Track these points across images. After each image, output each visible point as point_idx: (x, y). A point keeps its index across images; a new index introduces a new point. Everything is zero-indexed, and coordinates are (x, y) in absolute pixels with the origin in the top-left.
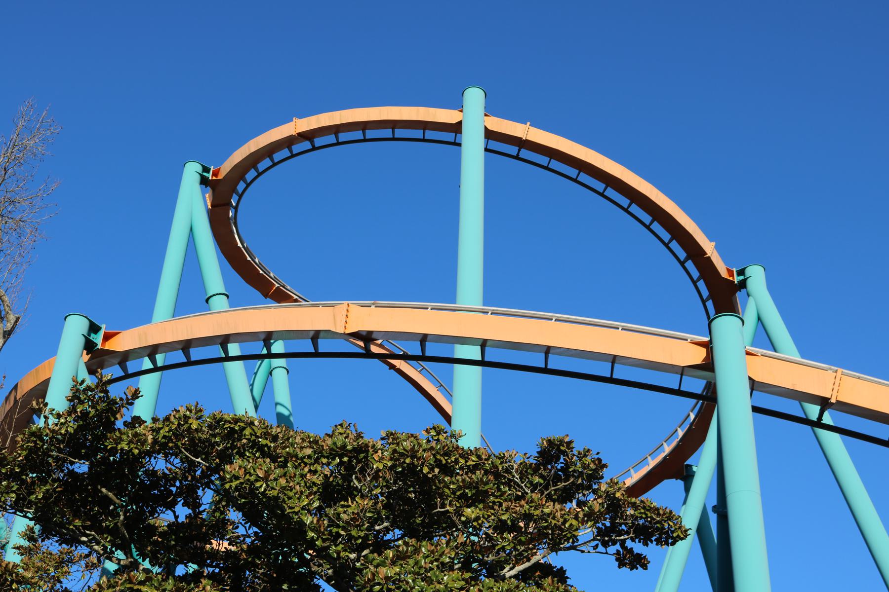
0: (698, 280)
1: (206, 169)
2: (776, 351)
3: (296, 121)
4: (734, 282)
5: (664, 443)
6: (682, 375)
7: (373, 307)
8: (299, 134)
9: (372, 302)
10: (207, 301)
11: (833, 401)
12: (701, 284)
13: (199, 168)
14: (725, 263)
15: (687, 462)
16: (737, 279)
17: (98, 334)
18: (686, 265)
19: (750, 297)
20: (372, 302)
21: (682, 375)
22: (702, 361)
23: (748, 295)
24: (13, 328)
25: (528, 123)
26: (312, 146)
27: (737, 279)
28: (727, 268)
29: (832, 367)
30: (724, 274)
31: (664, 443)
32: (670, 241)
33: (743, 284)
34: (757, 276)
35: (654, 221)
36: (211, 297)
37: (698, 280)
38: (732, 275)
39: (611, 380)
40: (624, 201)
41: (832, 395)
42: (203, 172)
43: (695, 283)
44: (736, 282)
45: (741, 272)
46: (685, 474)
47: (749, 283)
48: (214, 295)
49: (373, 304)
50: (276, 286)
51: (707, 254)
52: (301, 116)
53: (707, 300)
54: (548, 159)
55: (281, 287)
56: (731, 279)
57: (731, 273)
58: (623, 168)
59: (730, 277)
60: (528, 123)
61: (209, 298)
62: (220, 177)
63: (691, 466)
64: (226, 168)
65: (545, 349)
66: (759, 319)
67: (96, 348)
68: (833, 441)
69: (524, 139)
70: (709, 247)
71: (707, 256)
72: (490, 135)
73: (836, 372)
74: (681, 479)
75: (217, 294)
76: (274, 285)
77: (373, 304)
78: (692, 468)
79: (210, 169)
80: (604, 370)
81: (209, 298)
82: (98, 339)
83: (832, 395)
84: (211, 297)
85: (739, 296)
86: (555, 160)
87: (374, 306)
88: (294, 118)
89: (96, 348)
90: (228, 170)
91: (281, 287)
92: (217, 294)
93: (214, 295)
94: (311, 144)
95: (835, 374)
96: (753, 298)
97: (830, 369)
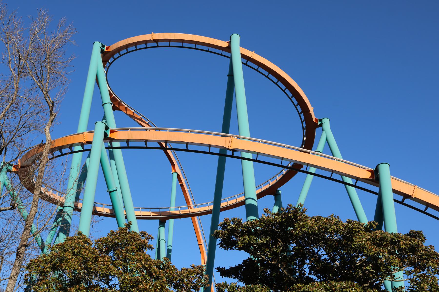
0: (297, 105)
1: (103, 46)
2: (333, 156)
3: (153, 34)
4: (318, 124)
5: (270, 180)
6: (282, 160)
7: (236, 138)
8: (154, 40)
9: (236, 135)
10: (103, 105)
11: (413, 197)
12: (298, 107)
13: (100, 45)
14: (315, 116)
15: (278, 189)
16: (319, 123)
17: (107, 130)
18: (301, 115)
19: (324, 131)
20: (236, 135)
21: (282, 160)
22: (370, 177)
23: (323, 130)
24: (54, 119)
25: (254, 52)
26: (157, 45)
27: (319, 123)
28: (315, 118)
29: (409, 183)
30: (314, 120)
31: (270, 180)
32: (285, 89)
33: (321, 125)
34: (327, 123)
35: (158, 43)
36: (105, 104)
37: (297, 105)
38: (317, 122)
39: (330, 179)
40: (266, 73)
41: (413, 195)
42: (102, 47)
43: (296, 106)
44: (318, 124)
45: (321, 120)
46: (276, 194)
47: (324, 125)
48: (107, 103)
49: (236, 136)
50: (113, 96)
51: (310, 112)
52: (155, 32)
53: (304, 121)
54: (222, 51)
55: (116, 97)
56: (316, 122)
57: (316, 120)
58: (287, 74)
59: (316, 121)
60: (254, 52)
61: (104, 104)
62: (108, 50)
63: (278, 190)
64: (113, 47)
65: (209, 146)
66: (327, 140)
67: (107, 137)
68: (352, 190)
69: (252, 58)
70: (311, 109)
71: (310, 113)
72: (243, 56)
73: (415, 186)
74: (274, 195)
75: (108, 103)
76: (112, 95)
77: (236, 136)
78: (279, 191)
79: (105, 46)
80: (328, 174)
81: (104, 104)
82: (108, 132)
83: (413, 195)
84: (105, 104)
85: (317, 130)
86: (261, 67)
87: (237, 137)
88: (152, 33)
89: (107, 137)
90: (114, 48)
91: (116, 97)
92: (108, 103)
93: (107, 103)
94: (157, 44)
95: (414, 187)
96: (325, 131)
97: (408, 183)
